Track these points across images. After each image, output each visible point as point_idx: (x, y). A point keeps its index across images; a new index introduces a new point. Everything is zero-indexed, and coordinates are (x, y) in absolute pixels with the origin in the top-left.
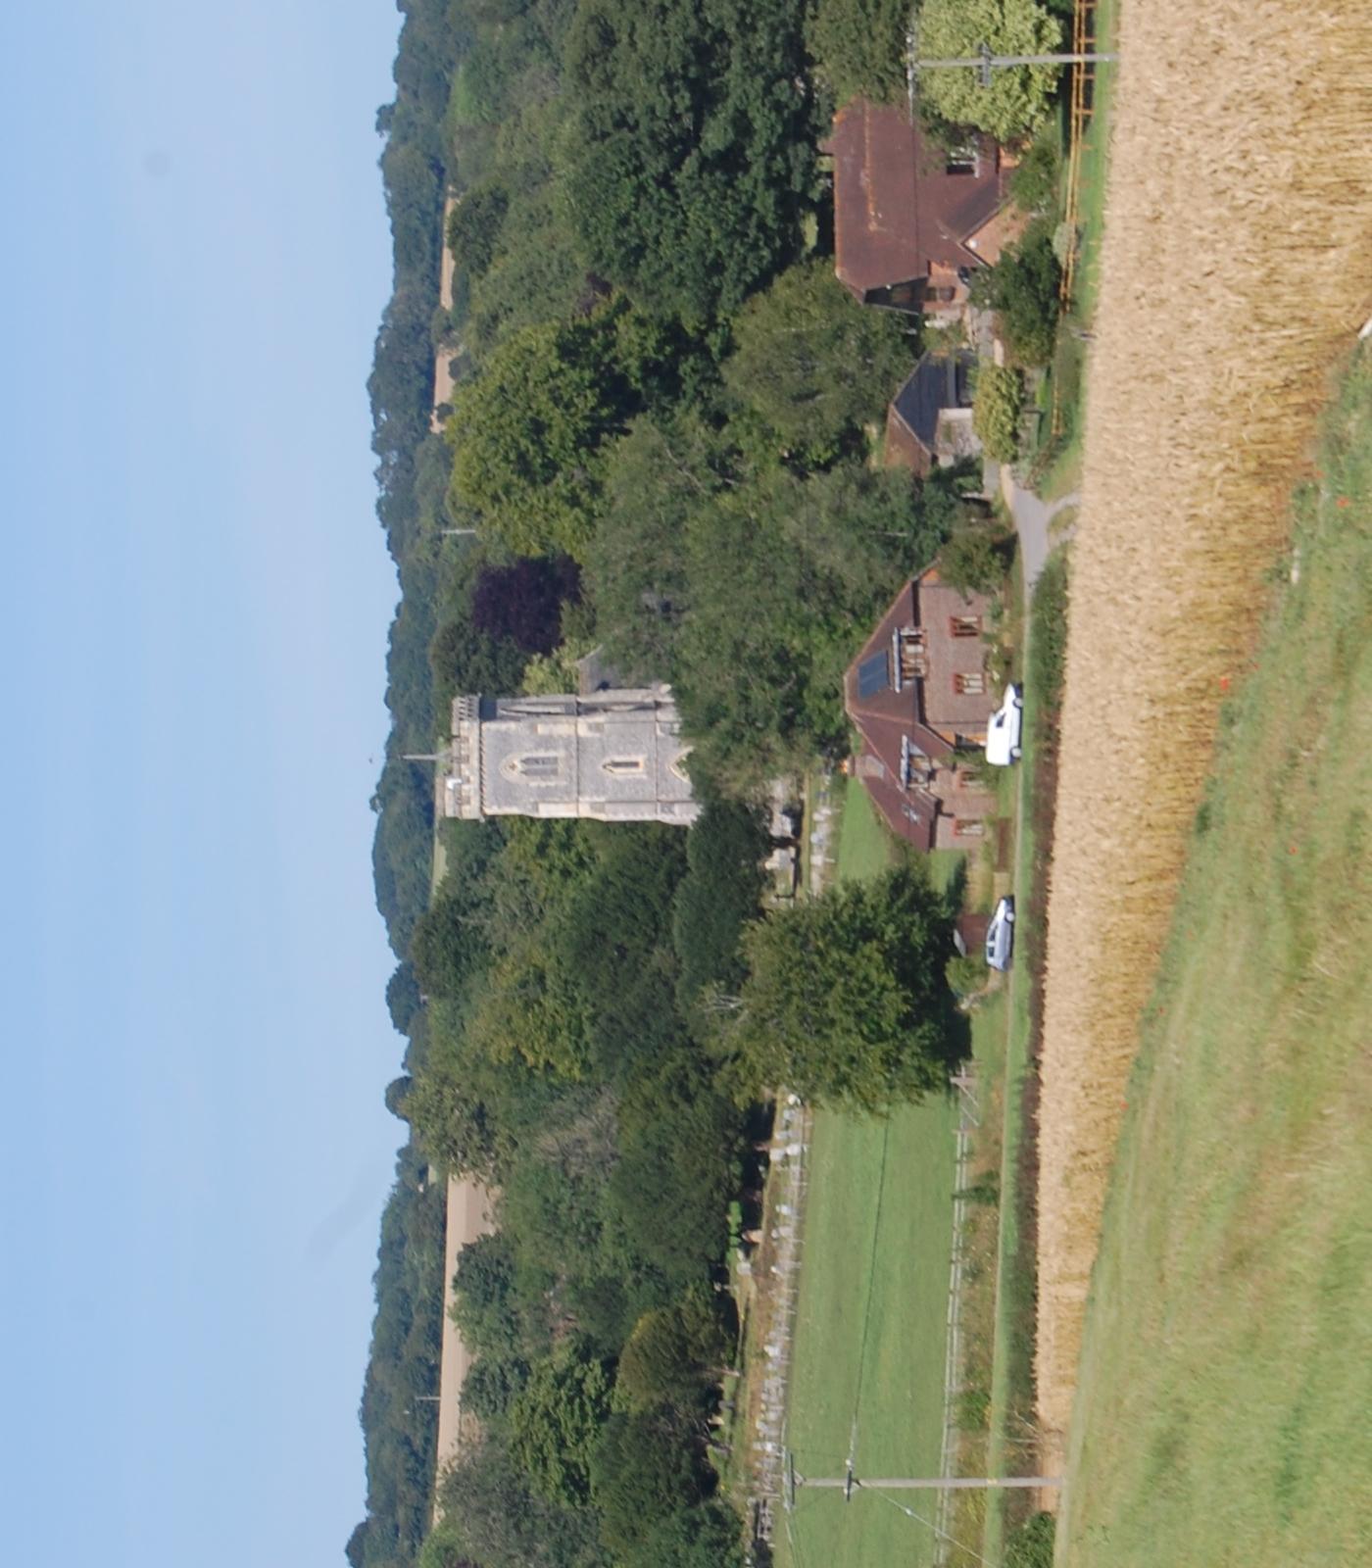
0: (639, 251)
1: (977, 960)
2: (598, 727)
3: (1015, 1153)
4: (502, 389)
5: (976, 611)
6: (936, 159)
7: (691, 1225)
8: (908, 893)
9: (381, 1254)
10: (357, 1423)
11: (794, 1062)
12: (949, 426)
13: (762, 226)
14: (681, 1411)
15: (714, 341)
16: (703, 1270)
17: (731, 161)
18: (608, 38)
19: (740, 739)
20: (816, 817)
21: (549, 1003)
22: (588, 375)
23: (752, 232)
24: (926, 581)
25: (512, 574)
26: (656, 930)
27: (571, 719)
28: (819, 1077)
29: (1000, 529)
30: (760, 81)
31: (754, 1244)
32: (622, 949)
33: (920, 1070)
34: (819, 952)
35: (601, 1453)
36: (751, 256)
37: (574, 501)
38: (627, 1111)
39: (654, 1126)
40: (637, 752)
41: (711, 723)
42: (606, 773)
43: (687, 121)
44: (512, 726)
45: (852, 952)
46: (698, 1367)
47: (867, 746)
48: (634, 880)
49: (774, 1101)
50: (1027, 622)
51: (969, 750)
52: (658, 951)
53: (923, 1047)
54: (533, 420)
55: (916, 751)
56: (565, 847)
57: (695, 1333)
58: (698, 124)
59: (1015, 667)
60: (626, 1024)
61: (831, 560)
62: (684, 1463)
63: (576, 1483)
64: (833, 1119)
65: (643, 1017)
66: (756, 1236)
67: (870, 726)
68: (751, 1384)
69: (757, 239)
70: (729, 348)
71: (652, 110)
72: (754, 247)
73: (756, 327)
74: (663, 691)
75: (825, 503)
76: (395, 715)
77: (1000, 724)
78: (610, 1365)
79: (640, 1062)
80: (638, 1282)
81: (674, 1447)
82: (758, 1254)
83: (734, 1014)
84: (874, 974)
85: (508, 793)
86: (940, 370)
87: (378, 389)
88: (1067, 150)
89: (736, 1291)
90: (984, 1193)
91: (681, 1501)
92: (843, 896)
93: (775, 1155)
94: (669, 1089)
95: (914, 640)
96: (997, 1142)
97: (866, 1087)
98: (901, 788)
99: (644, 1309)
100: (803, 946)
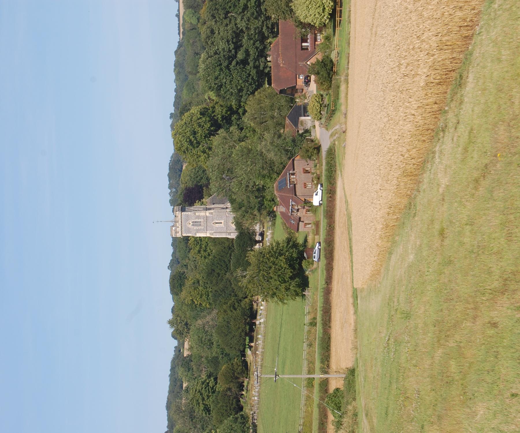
0: (221, 86)
1: (310, 260)
2: (211, 213)
3: (322, 309)
4: (185, 123)
5: (310, 166)
6: (299, 35)
7: (236, 342)
8: (291, 243)
9: (171, 370)
10: (165, 409)
11: (261, 289)
12: (302, 122)
13: (253, 79)
14: (233, 389)
15: (241, 111)
16: (239, 353)
17: (244, 62)
18: (212, 32)
19: (247, 212)
20: (267, 234)
21: (200, 288)
22: (208, 119)
23: (250, 80)
24: (296, 159)
25: (193, 189)
26: (227, 269)
27: (205, 211)
28: (268, 293)
29: (317, 144)
30: (252, 42)
31: (252, 347)
32: (219, 274)
33: (295, 291)
34: (267, 258)
35: (213, 401)
36: (250, 87)
37: (204, 152)
38: (220, 313)
39: (226, 316)
40: (222, 219)
41: (240, 208)
42: (214, 225)
43: (233, 52)
44: (190, 213)
45: (277, 258)
46: (237, 378)
47: (281, 203)
48: (222, 257)
49: (257, 309)
50: (324, 167)
51: (307, 203)
52: (228, 274)
53: (296, 285)
54: (193, 131)
55: (293, 203)
56: (205, 251)
57: (237, 369)
58: (236, 53)
59: (320, 179)
60: (219, 292)
61: (271, 156)
62: (234, 403)
63: (207, 410)
64: (273, 303)
65: (223, 290)
66: (252, 344)
67: (281, 197)
68: (251, 382)
69: (251, 82)
70: (245, 112)
71: (224, 49)
72: (251, 84)
73: (251, 105)
74: (229, 205)
75: (269, 141)
76: (174, 248)
77: (316, 195)
78: (216, 379)
79: (223, 301)
80: (223, 357)
81: (231, 398)
82: (253, 349)
83: (245, 276)
84: (283, 264)
85: (189, 230)
86: (300, 107)
87: (170, 176)
88: (334, 34)
89: (248, 359)
90: (313, 324)
91: (233, 413)
92: (274, 244)
93: (257, 323)
94: (230, 307)
95: (293, 174)
96: (316, 309)
97: (281, 296)
98: (290, 214)
99: (224, 364)
100: (263, 257)
